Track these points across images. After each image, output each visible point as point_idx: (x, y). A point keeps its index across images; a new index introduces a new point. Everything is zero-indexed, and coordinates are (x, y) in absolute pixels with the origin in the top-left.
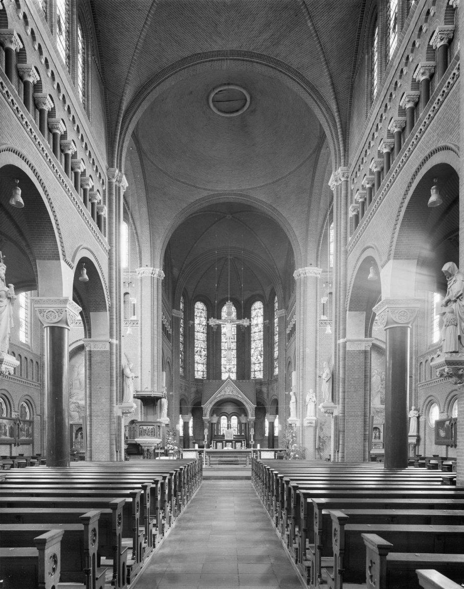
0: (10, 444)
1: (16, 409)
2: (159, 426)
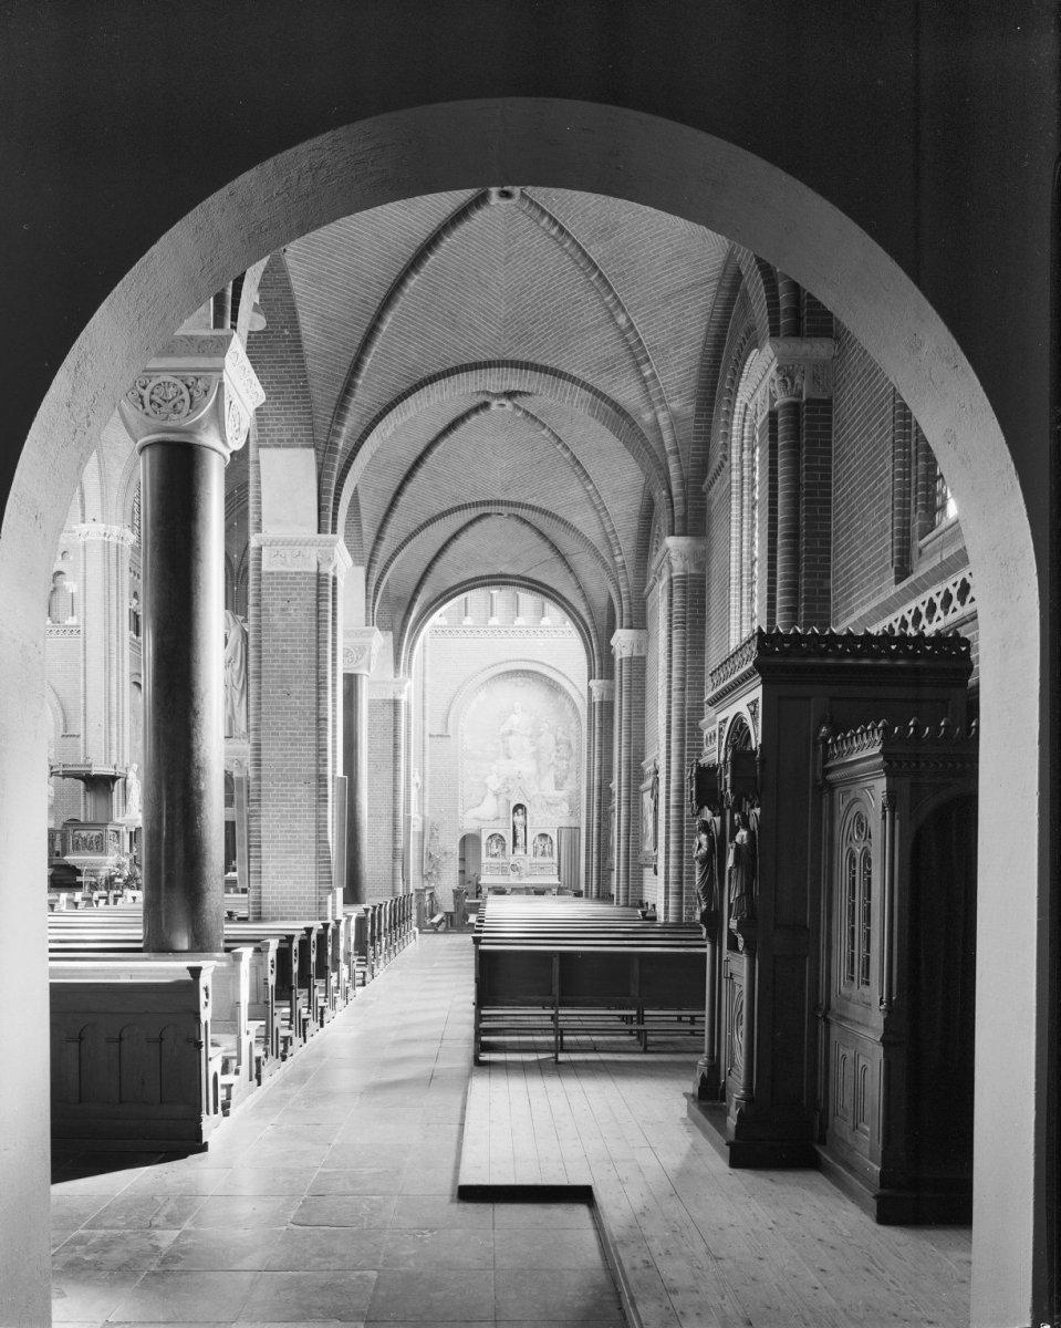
2: (117, 832)
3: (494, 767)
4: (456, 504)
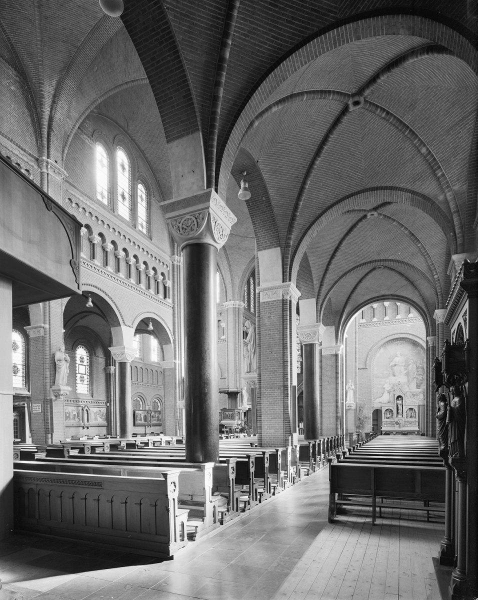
0: (145, 426)
1: (149, 404)
3: (388, 380)
4: (356, 265)
